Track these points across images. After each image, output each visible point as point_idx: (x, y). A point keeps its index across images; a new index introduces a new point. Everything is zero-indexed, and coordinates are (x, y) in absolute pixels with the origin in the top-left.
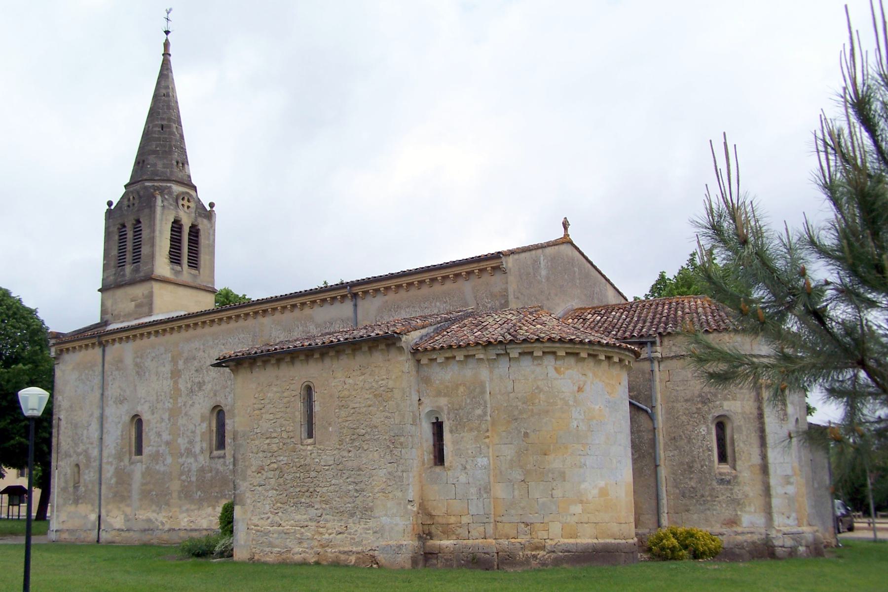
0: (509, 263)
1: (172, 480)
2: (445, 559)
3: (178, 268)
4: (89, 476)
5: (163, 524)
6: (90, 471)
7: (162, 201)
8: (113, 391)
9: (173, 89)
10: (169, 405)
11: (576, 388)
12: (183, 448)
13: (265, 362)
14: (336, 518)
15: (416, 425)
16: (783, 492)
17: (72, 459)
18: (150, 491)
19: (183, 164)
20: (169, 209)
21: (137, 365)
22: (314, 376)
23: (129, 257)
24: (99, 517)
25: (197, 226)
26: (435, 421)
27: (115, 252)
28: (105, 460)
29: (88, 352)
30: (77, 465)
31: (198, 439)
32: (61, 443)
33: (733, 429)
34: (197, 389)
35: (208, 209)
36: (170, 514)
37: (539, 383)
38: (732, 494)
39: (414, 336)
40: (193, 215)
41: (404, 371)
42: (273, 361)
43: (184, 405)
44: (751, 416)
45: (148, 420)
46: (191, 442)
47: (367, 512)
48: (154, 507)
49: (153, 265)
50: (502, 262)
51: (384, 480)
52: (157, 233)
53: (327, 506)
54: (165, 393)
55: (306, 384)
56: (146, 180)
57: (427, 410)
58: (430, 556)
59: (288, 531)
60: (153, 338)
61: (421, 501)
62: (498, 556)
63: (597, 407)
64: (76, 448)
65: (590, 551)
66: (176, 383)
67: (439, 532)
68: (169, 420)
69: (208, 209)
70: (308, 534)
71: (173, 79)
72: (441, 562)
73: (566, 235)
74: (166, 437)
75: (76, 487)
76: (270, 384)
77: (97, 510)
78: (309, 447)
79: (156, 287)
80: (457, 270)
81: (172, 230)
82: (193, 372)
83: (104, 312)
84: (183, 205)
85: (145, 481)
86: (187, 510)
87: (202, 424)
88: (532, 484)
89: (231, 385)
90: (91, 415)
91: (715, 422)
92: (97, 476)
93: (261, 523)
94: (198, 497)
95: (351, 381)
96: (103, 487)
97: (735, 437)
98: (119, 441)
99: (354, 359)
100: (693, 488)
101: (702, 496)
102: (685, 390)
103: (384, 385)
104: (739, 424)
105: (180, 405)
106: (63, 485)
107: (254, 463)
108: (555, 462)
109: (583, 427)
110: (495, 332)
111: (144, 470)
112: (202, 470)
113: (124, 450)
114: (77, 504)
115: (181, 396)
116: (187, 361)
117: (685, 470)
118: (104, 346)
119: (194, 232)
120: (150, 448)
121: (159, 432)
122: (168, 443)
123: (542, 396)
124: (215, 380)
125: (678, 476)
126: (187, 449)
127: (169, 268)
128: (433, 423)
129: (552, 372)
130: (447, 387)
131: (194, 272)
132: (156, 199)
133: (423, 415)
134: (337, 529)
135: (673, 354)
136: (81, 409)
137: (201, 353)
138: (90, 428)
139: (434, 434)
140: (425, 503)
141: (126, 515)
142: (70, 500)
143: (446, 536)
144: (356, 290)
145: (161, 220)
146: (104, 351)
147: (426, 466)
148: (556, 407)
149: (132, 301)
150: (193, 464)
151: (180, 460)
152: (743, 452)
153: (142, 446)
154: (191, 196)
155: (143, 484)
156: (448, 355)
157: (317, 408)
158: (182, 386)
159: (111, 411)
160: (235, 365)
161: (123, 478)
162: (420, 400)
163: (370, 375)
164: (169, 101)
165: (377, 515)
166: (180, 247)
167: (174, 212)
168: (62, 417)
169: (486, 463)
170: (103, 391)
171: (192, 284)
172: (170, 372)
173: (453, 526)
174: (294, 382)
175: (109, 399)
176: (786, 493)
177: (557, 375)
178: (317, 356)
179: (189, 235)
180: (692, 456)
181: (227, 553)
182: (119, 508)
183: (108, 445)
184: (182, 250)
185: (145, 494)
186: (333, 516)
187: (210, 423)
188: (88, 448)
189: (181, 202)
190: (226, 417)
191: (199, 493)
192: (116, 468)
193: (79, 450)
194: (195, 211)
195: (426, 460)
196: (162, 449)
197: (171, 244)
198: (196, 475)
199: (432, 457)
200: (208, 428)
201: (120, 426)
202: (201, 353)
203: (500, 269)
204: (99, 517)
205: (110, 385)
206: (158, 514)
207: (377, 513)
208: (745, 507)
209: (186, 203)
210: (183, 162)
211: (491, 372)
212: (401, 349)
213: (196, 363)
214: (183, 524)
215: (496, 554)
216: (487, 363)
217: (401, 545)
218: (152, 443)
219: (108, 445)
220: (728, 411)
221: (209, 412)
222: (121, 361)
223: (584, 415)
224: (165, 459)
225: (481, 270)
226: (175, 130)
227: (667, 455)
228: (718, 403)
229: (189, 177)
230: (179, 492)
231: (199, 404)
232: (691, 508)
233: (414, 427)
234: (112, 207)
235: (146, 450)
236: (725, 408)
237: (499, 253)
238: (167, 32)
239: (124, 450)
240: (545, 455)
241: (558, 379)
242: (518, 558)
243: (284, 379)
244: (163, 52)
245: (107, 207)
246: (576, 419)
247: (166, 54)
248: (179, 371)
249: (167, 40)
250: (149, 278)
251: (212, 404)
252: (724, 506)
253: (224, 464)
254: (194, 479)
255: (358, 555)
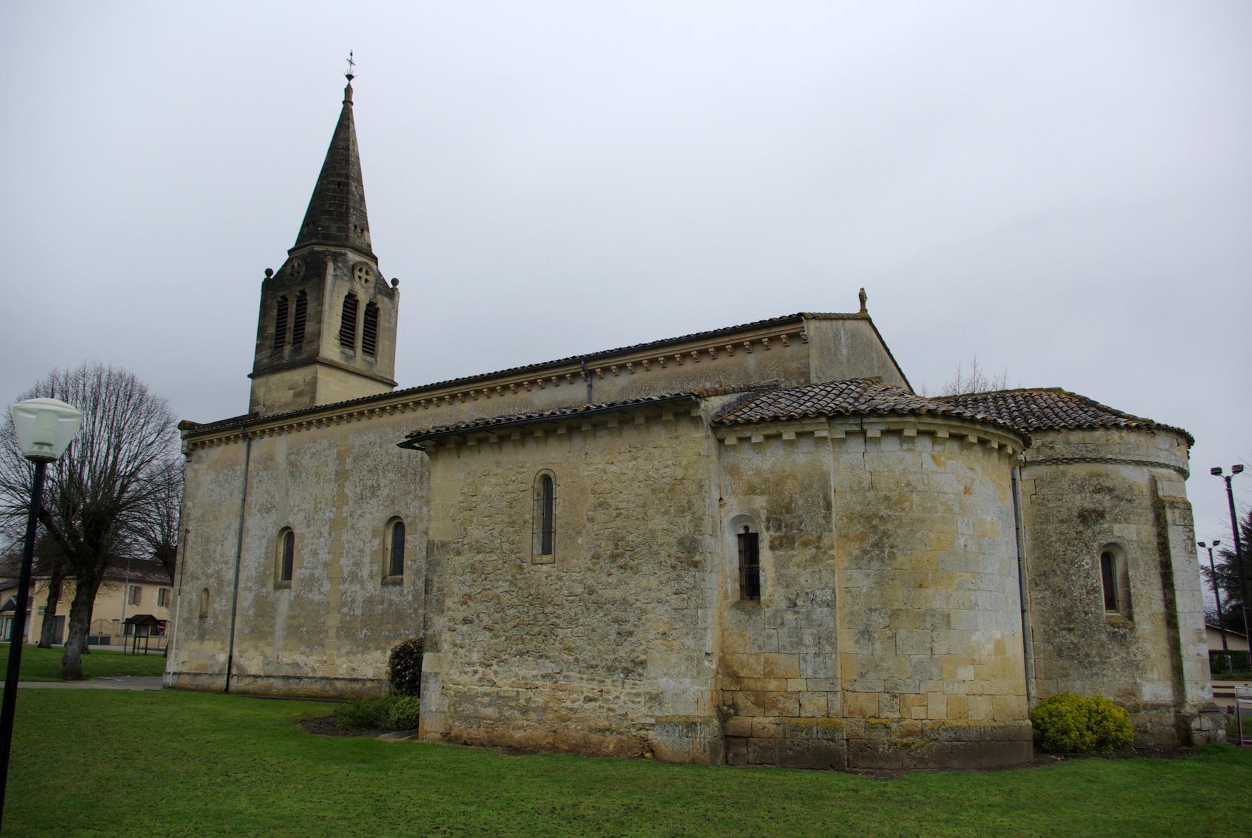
0: (811, 328)
1: (329, 613)
2: (760, 747)
3: (350, 352)
4: (220, 605)
5: (314, 670)
6: (221, 599)
7: (335, 270)
8: (256, 497)
9: (355, 142)
10: (331, 515)
11: (962, 489)
12: (346, 571)
13: (481, 442)
14: (585, 676)
15: (716, 537)
16: (1196, 653)
17: (200, 582)
18: (301, 626)
19: (362, 230)
20: (343, 279)
21: (291, 464)
22: (556, 461)
23: (289, 336)
24: (231, 657)
25: (376, 304)
26: (742, 531)
27: (272, 330)
28: (241, 585)
29: (228, 446)
30: (206, 590)
31: (367, 560)
32: (187, 561)
33: (1126, 563)
34: (368, 495)
35: (391, 286)
36: (325, 658)
37: (911, 477)
38: (1128, 653)
39: (714, 404)
40: (372, 291)
41: (702, 454)
42: (493, 439)
43: (351, 515)
44: (1149, 546)
45: (302, 534)
46: (357, 564)
47: (634, 668)
48: (303, 648)
49: (319, 346)
50: (803, 327)
51: (666, 620)
52: (326, 307)
53: (571, 657)
54: (326, 499)
55: (543, 472)
56: (316, 244)
57: (732, 515)
58: (736, 740)
59: (506, 695)
60: (313, 429)
61: (721, 654)
62: (848, 745)
63: (989, 519)
64: (206, 569)
65: (989, 739)
66: (341, 486)
67: (750, 703)
68: (330, 534)
69: (391, 286)
70: (538, 699)
71: (354, 131)
72: (754, 751)
73: (863, 309)
74: (324, 556)
75: (203, 617)
76: (486, 473)
77: (228, 649)
78: (544, 567)
79: (322, 372)
80: (736, 338)
81: (344, 306)
82: (365, 472)
83: (254, 402)
84: (360, 277)
85: (293, 613)
86: (348, 653)
87: (373, 540)
88: (902, 633)
89: (415, 490)
90: (228, 527)
91: (1101, 553)
92: (231, 604)
93: (464, 679)
94: (363, 636)
95: (614, 468)
96: (238, 619)
97: (1130, 573)
98: (263, 561)
99: (621, 434)
100: (1073, 644)
101: (1088, 655)
102: (1058, 507)
103: (668, 474)
104: (1134, 556)
105: (345, 515)
106: (186, 615)
107: (457, 591)
108: (935, 598)
109: (973, 547)
110: (211, 672)
111: (292, 599)
112: (370, 601)
113: (268, 572)
114: (202, 641)
115: (347, 504)
116: (356, 459)
117: (1061, 618)
118: (250, 439)
119: (372, 311)
120: (303, 570)
121: (316, 550)
122: (326, 565)
123: (914, 497)
124: (394, 483)
125: (1051, 627)
126: (351, 573)
127: (339, 350)
128: (740, 536)
129: (928, 463)
130: (766, 481)
131: (369, 358)
132: (326, 265)
133: (726, 523)
134: (585, 694)
135: (1041, 457)
136: (216, 518)
137: (377, 448)
138: (225, 543)
139: (740, 552)
140: (728, 657)
141: (265, 657)
142: (194, 634)
143: (763, 710)
144: (591, 366)
145: (333, 292)
146: (249, 446)
147: (730, 600)
148: (936, 515)
149: (290, 389)
150: (358, 593)
151: (341, 587)
152: (1142, 595)
153: (291, 568)
154: (370, 267)
155: (290, 617)
156: (772, 431)
157: (558, 510)
158: (349, 491)
159: (254, 522)
160: (434, 446)
161: (264, 609)
162: (721, 499)
163: (646, 459)
164: (348, 156)
165: (653, 674)
166: (353, 335)
167: (348, 285)
168: (190, 528)
169: (829, 597)
170: (245, 494)
171: (367, 374)
172: (334, 473)
173: (774, 694)
174: (524, 470)
175: (253, 506)
176: (1198, 654)
177: (934, 467)
178: (562, 431)
179: (366, 314)
180: (1071, 599)
181: (411, 725)
182: (256, 648)
183: (247, 566)
184: (356, 332)
185: (293, 631)
186: (580, 673)
187: (384, 540)
188: (221, 569)
189: (357, 274)
190: (406, 533)
191: (365, 631)
192: (256, 596)
193: (210, 571)
194: (375, 287)
195: (729, 591)
196: (318, 572)
197: (342, 323)
198: (362, 607)
199: (737, 586)
200: (382, 546)
201: (264, 542)
202: (377, 448)
203: (800, 336)
204: (231, 657)
205: (255, 489)
206: (308, 657)
207: (652, 670)
208: (1146, 673)
209: (363, 274)
210: (364, 228)
211: (836, 459)
212: (697, 420)
213: (369, 461)
214: (341, 672)
215: (845, 742)
216: (830, 444)
217: (692, 723)
218: (305, 564)
219: (247, 566)
220: (1119, 537)
221: (383, 525)
222: (271, 458)
223: (974, 529)
224: (322, 586)
225: (771, 339)
226: (354, 189)
227: (1033, 597)
228: (1106, 526)
229: (369, 246)
230: (339, 629)
231: (371, 513)
232: (1071, 672)
233: (713, 538)
234: (272, 277)
235: (297, 573)
236: (1116, 533)
237: (800, 314)
238: (350, 77)
239: (268, 572)
240: (921, 586)
241: (937, 473)
242: (881, 749)
243: (508, 467)
244: (343, 99)
245: (265, 276)
246: (963, 535)
247: (348, 103)
248: (347, 471)
249: (349, 86)
250: (314, 359)
251: (389, 513)
252: (1118, 670)
253: (401, 593)
254: (358, 612)
255: (620, 736)
